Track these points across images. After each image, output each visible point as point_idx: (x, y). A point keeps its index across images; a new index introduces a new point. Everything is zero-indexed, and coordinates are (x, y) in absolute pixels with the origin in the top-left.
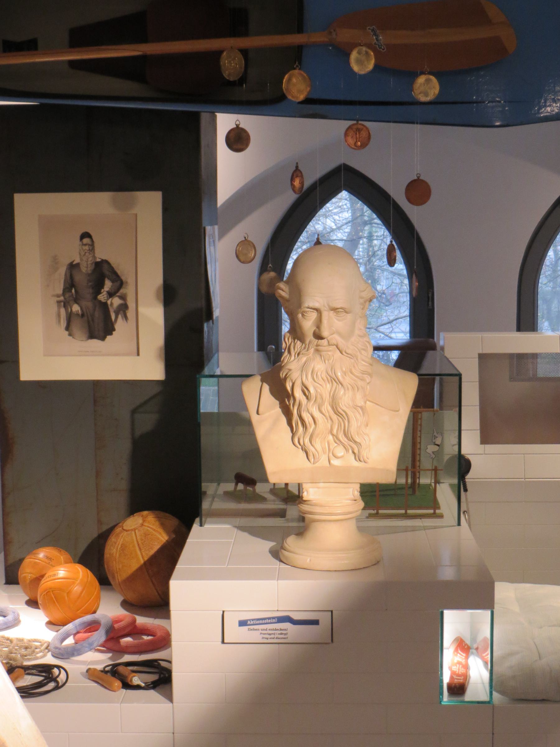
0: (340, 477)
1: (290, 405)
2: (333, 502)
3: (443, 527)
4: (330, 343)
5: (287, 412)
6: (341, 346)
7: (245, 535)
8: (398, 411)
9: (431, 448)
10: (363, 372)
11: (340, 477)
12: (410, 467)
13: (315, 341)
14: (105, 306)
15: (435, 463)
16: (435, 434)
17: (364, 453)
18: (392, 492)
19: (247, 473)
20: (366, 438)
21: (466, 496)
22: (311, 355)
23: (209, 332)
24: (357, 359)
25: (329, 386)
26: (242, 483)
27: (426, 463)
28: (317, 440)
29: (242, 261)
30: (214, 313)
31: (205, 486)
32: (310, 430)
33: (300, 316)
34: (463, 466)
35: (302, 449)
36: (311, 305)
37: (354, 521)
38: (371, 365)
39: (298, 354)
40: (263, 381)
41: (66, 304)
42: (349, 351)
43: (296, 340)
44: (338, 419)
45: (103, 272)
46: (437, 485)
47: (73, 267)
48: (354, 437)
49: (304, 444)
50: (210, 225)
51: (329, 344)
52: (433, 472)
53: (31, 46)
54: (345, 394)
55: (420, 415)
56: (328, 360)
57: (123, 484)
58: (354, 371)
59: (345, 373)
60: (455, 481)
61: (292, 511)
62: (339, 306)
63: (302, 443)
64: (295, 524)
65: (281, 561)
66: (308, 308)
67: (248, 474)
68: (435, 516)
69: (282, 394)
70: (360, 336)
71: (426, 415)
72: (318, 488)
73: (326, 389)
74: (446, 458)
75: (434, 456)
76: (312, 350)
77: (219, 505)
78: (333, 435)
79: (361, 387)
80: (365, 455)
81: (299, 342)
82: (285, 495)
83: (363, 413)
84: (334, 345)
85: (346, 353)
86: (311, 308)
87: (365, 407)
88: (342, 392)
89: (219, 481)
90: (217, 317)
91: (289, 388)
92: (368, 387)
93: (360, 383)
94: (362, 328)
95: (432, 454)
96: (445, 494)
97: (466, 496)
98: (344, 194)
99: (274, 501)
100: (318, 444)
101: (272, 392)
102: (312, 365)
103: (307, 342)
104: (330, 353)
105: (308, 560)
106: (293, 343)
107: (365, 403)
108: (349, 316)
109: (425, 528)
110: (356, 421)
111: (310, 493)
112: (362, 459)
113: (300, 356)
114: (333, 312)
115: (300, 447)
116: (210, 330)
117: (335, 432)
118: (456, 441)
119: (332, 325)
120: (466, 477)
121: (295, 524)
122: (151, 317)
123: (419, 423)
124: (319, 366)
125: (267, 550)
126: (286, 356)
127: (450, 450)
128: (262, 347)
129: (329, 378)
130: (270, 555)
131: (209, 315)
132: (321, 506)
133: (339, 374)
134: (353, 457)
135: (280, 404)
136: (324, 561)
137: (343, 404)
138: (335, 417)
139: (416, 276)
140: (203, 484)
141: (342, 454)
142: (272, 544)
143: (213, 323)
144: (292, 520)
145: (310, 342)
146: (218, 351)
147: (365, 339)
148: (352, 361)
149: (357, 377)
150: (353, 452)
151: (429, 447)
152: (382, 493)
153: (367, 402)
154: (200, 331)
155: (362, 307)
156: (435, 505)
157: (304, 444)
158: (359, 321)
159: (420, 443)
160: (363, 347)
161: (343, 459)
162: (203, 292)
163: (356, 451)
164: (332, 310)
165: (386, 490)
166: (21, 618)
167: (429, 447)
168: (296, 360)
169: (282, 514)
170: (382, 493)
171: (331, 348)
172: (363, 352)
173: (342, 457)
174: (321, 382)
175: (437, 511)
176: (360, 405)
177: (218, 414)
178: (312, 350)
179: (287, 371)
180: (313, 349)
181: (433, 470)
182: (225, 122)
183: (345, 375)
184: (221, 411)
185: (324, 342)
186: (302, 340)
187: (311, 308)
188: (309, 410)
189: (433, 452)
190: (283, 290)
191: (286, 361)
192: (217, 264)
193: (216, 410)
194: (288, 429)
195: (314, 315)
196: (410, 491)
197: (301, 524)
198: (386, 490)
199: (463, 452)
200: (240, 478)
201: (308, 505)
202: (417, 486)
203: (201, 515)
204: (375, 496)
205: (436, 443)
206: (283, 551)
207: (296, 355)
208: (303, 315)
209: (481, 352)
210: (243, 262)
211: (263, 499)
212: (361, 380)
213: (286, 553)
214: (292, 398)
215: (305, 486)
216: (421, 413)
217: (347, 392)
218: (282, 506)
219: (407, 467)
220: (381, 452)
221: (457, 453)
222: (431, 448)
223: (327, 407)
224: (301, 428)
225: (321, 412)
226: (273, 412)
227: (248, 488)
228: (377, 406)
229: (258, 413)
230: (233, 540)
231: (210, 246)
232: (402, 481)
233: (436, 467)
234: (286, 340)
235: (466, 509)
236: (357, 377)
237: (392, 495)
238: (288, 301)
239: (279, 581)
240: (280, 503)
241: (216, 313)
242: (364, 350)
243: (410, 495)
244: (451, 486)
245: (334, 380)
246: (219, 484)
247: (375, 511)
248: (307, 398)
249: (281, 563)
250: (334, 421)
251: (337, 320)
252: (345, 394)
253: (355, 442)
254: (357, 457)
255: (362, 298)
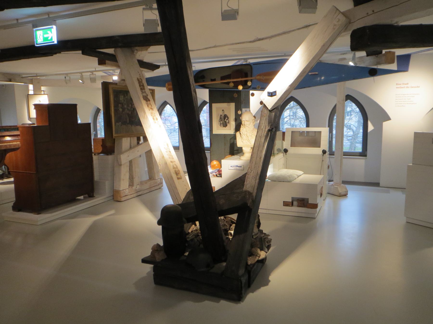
14: (226, 122)
41: (220, 121)
45: (225, 116)
47: (221, 115)
53: (214, 80)
57: (229, 151)
119: (246, 123)
122: (233, 124)
166: (348, 193)
182: (251, 92)
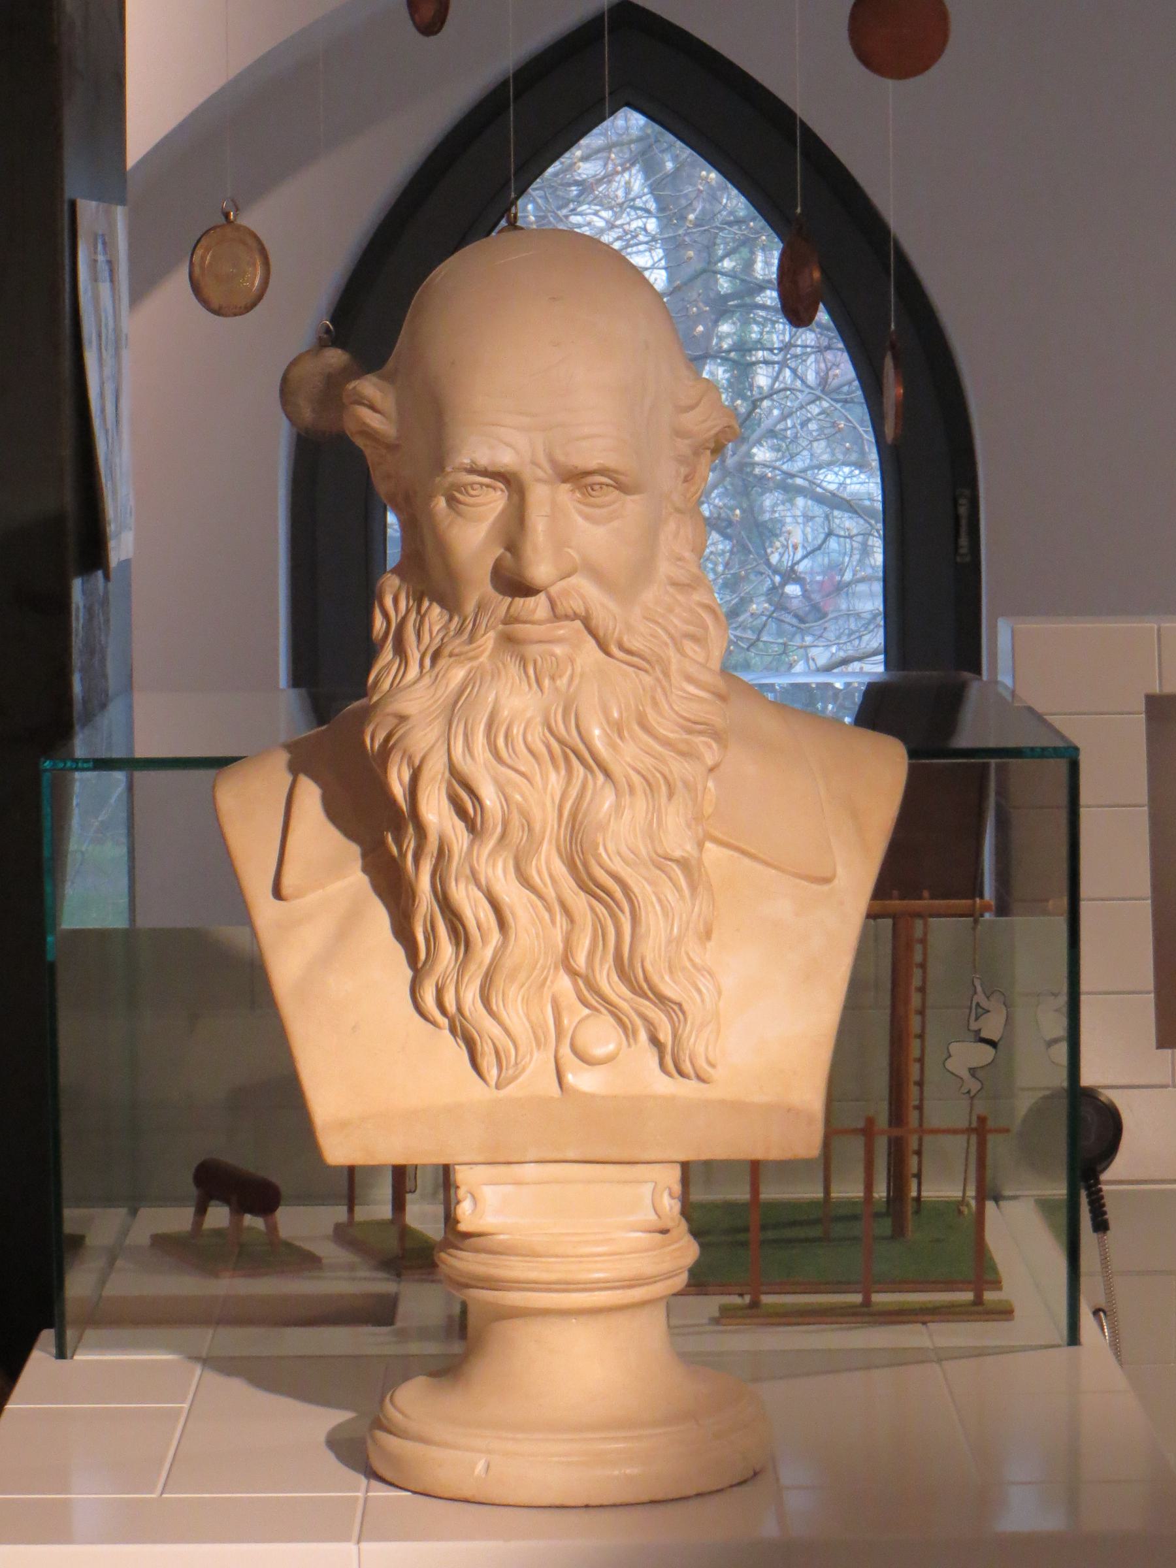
0: (601, 1139)
1: (403, 855)
2: (577, 1238)
3: (1011, 1350)
4: (560, 610)
5: (392, 887)
6: (600, 618)
7: (238, 1389)
8: (826, 880)
9: (967, 1056)
10: (692, 726)
11: (601, 1139)
12: (882, 1121)
13: (502, 604)
15: (981, 1108)
16: (980, 998)
17: (697, 1045)
18: (816, 1232)
19: (245, 1158)
20: (704, 983)
21: (1102, 1245)
22: (484, 659)
23: (89, 610)
24: (666, 674)
25: (555, 780)
26: (226, 1201)
27: (943, 1108)
28: (512, 991)
29: (216, 302)
30: (112, 544)
31: (72, 1217)
32: (485, 954)
33: (441, 503)
34: (1089, 1132)
35: (453, 1030)
36: (483, 457)
37: (658, 1316)
38: (723, 698)
39: (436, 656)
40: (296, 768)
42: (635, 644)
43: (426, 603)
44: (592, 909)
46: (990, 1205)
48: (655, 979)
49: (459, 1009)
50: (99, 199)
51: (557, 616)
52: (974, 1139)
54: (618, 808)
55: (919, 923)
56: (553, 678)
58: (652, 717)
59: (618, 728)
60: (1059, 1190)
61: (421, 1303)
62: (593, 464)
63: (451, 1007)
64: (432, 1348)
65: (372, 1474)
66: (472, 471)
67: (251, 1172)
68: (979, 1310)
69: (375, 821)
70: (674, 584)
71: (943, 933)
72: (517, 1183)
73: (544, 793)
74: (1023, 1104)
75: (974, 1086)
76: (488, 640)
77: (131, 1283)
78: (573, 973)
79: (686, 784)
80: (700, 1050)
81: (436, 610)
82: (391, 1243)
83: (693, 888)
84: (576, 616)
85: (621, 647)
86: (484, 473)
87: (700, 861)
88: (608, 800)
89: (134, 1202)
90: (126, 564)
91: (398, 791)
92: (710, 784)
93: (679, 768)
94: (687, 554)
95: (965, 1074)
96: (1021, 1236)
97: (1102, 1245)
98: (629, 122)
99: (352, 1267)
100: (514, 1008)
101: (334, 812)
102: (491, 698)
103: (470, 607)
104: (558, 650)
105: (480, 1467)
106: (413, 616)
107: (700, 846)
108: (633, 505)
109: (941, 1356)
110: (663, 918)
111: (490, 1204)
112: (687, 1067)
113: (442, 663)
114: (568, 486)
115: (444, 1022)
116: (99, 605)
117: (580, 960)
118: (1058, 1027)
119: (570, 539)
120: (1104, 1177)
121: (432, 1348)
123: (918, 958)
124: (517, 700)
125: (322, 1438)
126: (388, 665)
127: (1038, 1074)
128: (305, 672)
129: (555, 746)
130: (330, 1457)
131: (92, 550)
132: (532, 1254)
133: (597, 732)
134: (651, 1059)
135: (364, 856)
136: (542, 1466)
137: (611, 847)
138: (579, 902)
139: (896, 358)
140: (67, 1213)
141: (611, 1047)
142: (338, 1417)
143: (107, 577)
144: (424, 1334)
145: (480, 607)
146: (128, 687)
147: (696, 597)
148: (647, 679)
149: (666, 743)
150: (655, 1041)
151: (954, 1048)
152: (770, 1234)
153: (708, 845)
154: (58, 606)
155: (683, 470)
156: (983, 1273)
157: (459, 1009)
158: (672, 526)
159: (921, 1036)
160: (691, 629)
161: (616, 1068)
162: (67, 452)
163: (665, 1036)
164: (564, 481)
165: (794, 1224)
167: (954, 1048)
168: (426, 680)
169: (381, 1312)
170: (770, 1234)
171: (564, 629)
172: (689, 646)
173: (609, 1059)
174: (525, 763)
175: (989, 1296)
176: (678, 854)
177: (130, 935)
178: (488, 640)
179: (391, 722)
180: (492, 634)
181: (969, 1131)
183: (621, 736)
184: (143, 923)
185: (537, 606)
186: (450, 602)
187: (484, 473)
188: (483, 877)
189: (973, 1071)
190: (373, 408)
191: (386, 686)
192: (125, 353)
193: (119, 922)
194: (400, 953)
195: (492, 503)
196: (885, 1226)
197: (457, 1348)
198: (794, 1224)
199: (1088, 1079)
200: (216, 1182)
201: (477, 1251)
202: (910, 1208)
203: (62, 1315)
204: (744, 1244)
205: (984, 1034)
206: (381, 1435)
207: (427, 662)
208: (452, 501)
209: (1157, 690)
210: (217, 312)
211: (307, 1261)
212: (683, 754)
213: (392, 1443)
214: (411, 830)
215: (463, 1175)
216: (919, 915)
217: (626, 800)
218: (383, 1285)
219: (870, 1121)
220: (762, 1019)
221: (1061, 1080)
222: (967, 1056)
223: (548, 864)
224: (447, 949)
225: (525, 881)
226: (339, 885)
227: (249, 1220)
228: (746, 861)
229: (277, 893)
230: (186, 1406)
231: (95, 279)
232: (848, 1190)
233: (982, 1120)
234: (388, 602)
235: (1102, 1302)
236: (666, 743)
237: (813, 1240)
238: (393, 448)
239: (365, 1546)
240: (381, 1275)
241: (122, 546)
242: (694, 638)
243: (884, 1238)
244: (1045, 1206)
245: (575, 753)
246: (134, 1212)
247: (747, 1299)
248: (471, 826)
249: (375, 1483)
250: (577, 917)
251: (587, 518)
252: (618, 808)
253: (661, 1000)
254: (672, 1060)
255: (679, 433)
